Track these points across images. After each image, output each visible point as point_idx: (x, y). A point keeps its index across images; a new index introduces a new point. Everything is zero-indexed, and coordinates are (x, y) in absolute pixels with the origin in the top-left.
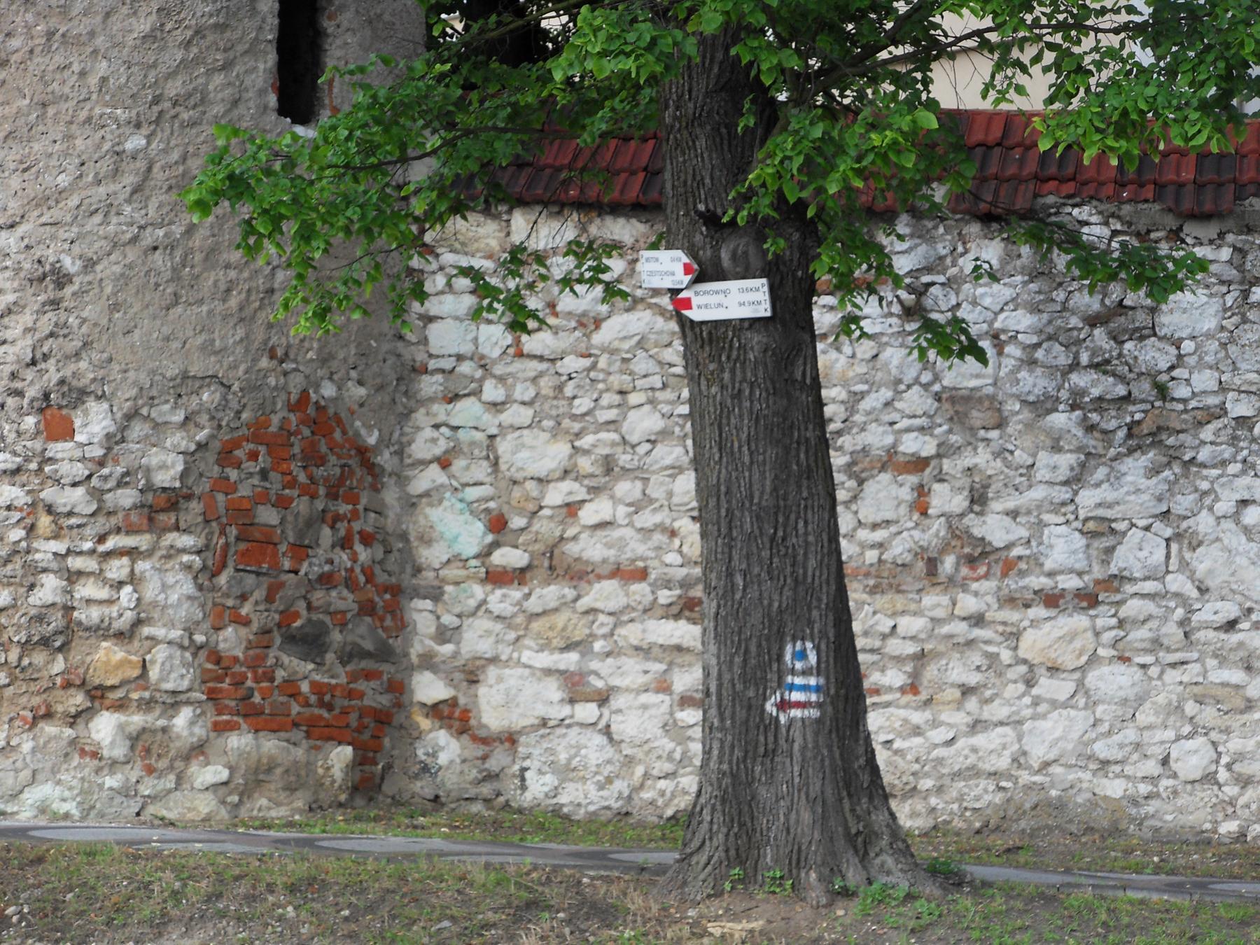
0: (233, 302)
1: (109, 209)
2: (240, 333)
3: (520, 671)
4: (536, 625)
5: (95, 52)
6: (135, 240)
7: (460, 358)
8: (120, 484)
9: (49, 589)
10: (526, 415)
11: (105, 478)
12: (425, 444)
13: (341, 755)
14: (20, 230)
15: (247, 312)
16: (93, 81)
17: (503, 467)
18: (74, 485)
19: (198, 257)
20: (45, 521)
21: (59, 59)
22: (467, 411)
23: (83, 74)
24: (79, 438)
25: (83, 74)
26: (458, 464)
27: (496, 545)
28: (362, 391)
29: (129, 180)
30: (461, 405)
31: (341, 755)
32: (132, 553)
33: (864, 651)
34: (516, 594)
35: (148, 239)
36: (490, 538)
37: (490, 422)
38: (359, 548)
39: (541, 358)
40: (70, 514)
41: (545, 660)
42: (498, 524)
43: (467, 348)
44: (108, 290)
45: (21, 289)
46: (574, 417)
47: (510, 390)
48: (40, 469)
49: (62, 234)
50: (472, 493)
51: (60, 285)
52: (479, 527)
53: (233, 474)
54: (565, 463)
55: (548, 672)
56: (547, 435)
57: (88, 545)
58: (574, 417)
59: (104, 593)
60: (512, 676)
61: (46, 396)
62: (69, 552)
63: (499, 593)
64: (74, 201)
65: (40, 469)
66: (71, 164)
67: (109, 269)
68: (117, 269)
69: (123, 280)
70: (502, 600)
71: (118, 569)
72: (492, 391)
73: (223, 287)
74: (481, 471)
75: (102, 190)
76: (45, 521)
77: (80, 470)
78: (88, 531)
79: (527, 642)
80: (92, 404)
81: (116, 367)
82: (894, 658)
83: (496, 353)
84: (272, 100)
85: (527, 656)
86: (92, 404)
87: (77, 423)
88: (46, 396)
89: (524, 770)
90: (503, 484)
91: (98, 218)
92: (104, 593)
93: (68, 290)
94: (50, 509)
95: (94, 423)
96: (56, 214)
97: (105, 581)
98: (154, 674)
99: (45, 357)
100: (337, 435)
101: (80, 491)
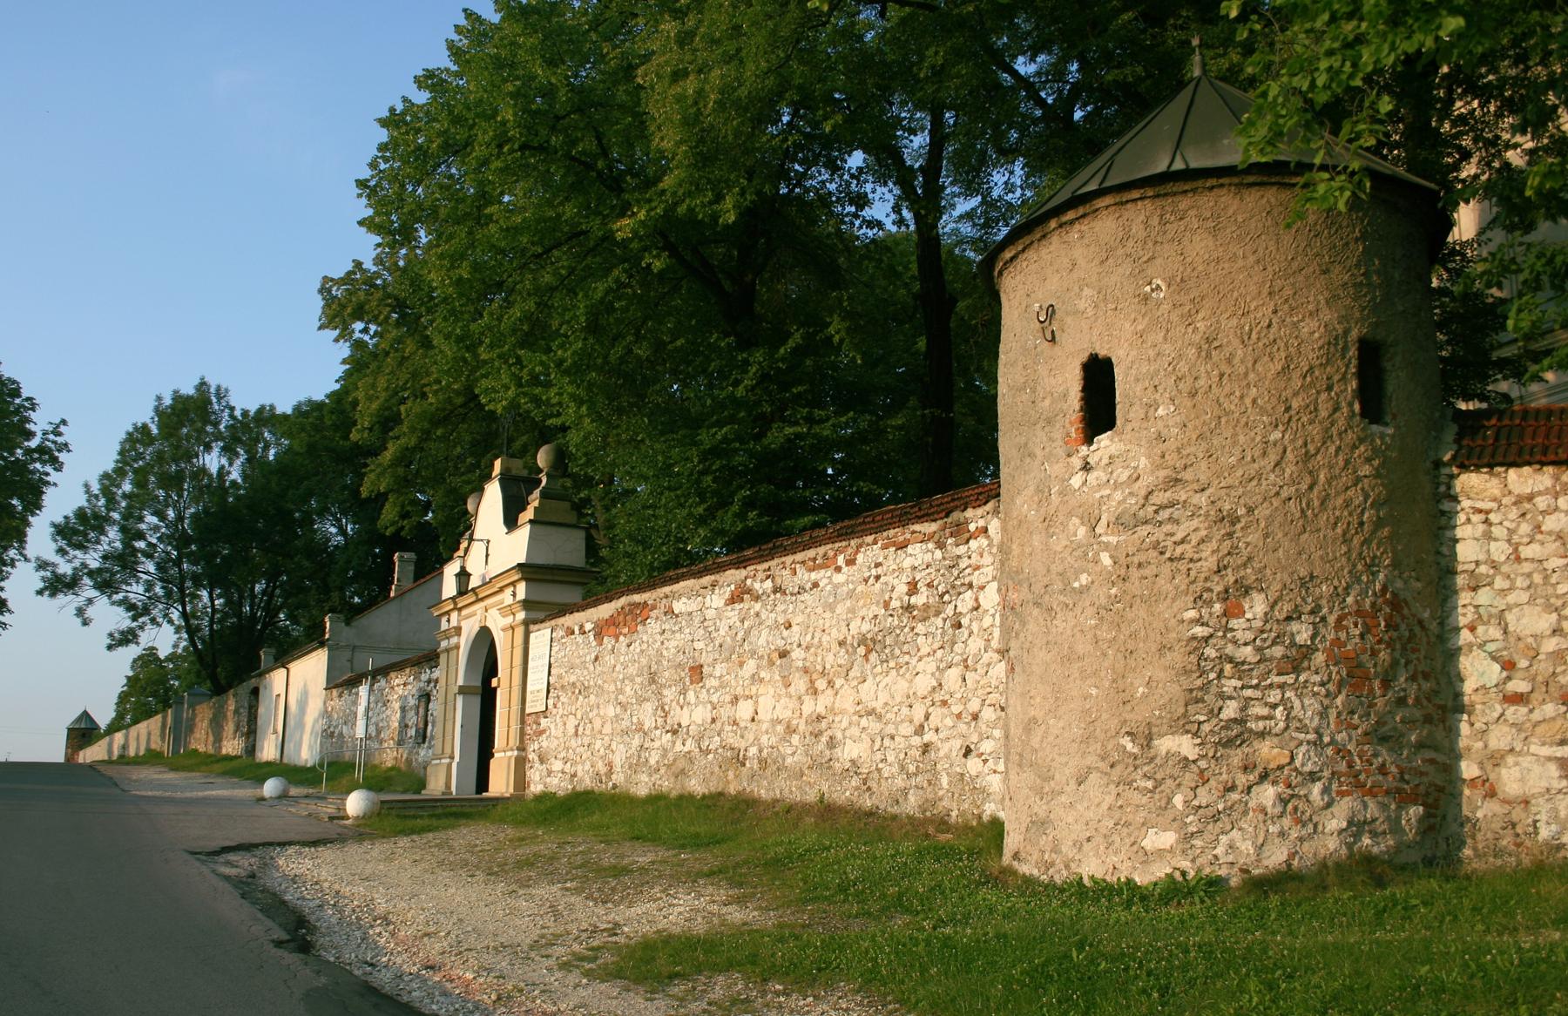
0: (1339, 530)
1: (1259, 476)
2: (1344, 549)
3: (1529, 758)
4: (1539, 730)
5: (1248, 385)
6: (1277, 494)
7: (1477, 563)
8: (1274, 643)
9: (1230, 710)
10: (1524, 597)
11: (1264, 640)
12: (1464, 617)
13: (1415, 811)
14: (1207, 492)
15: (1348, 536)
16: (1248, 401)
17: (1511, 628)
18: (1246, 644)
19: (1316, 503)
20: (1228, 667)
21: (1227, 389)
22: (1484, 597)
23: (1242, 397)
24: (1249, 615)
25: (1242, 397)
26: (1480, 629)
27: (1509, 678)
28: (1419, 585)
29: (1273, 457)
30: (1481, 591)
31: (1415, 811)
32: (1282, 686)
33: (127, 737)
34: (1524, 710)
35: (1285, 494)
36: (1505, 674)
37: (1501, 604)
38: (1421, 681)
39: (1533, 560)
40: (1243, 663)
41: (1546, 751)
42: (1509, 666)
43: (1482, 557)
44: (1262, 525)
45: (1210, 527)
46: (1558, 597)
47: (1513, 581)
48: (1224, 636)
49: (1233, 493)
50: (1491, 647)
51: (1233, 524)
52: (1497, 667)
53: (1343, 636)
54: (1554, 626)
55: (1549, 759)
56: (1539, 609)
57: (1255, 682)
58: (1558, 597)
59: (1265, 711)
60: (1526, 761)
61: (1226, 591)
62: (1242, 688)
63: (1513, 708)
64: (1239, 473)
65: (1224, 636)
66: (1237, 452)
67: (1262, 512)
68: (1268, 512)
69: (1270, 520)
70: (1516, 713)
71: (1274, 696)
72: (1499, 583)
73: (1332, 520)
74: (1494, 632)
75: (1256, 466)
76: (1228, 667)
77: (1249, 636)
78: (1255, 673)
79: (1533, 739)
80: (1255, 594)
81: (1268, 571)
82: (177, 741)
83: (1503, 558)
84: (975, 517)
85: (1533, 749)
86: (1255, 594)
87: (1247, 607)
88: (1226, 591)
89: (1536, 822)
90: (1512, 640)
91: (1254, 483)
92: (1265, 711)
93: (1238, 526)
94: (1231, 660)
95: (1257, 606)
96: (1229, 481)
97: (1266, 704)
98: (1298, 763)
99: (1225, 567)
100: (1406, 611)
101: (1249, 648)
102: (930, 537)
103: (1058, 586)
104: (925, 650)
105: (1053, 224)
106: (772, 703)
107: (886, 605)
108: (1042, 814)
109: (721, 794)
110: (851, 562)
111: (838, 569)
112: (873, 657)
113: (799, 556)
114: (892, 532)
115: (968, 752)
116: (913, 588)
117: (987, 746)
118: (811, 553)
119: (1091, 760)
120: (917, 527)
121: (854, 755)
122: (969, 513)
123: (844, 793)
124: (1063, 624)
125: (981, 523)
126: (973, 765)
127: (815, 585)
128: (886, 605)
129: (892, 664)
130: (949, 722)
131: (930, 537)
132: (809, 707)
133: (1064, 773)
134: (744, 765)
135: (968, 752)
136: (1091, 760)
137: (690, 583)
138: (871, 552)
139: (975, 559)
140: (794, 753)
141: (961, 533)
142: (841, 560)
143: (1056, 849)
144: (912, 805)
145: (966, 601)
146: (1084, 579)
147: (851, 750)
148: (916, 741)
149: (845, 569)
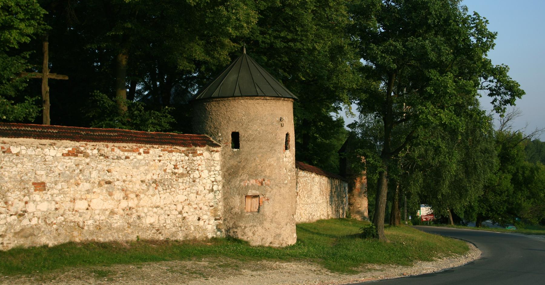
102: (183, 152)
103: (282, 182)
104: (182, 187)
105: (283, 99)
106: (100, 202)
107: (165, 170)
108: (279, 233)
109: (71, 243)
110: (147, 152)
111: (140, 154)
112: (160, 188)
113: (117, 144)
114: (166, 146)
115: (199, 219)
116: (175, 167)
117: (205, 217)
118: (124, 144)
119: (288, 220)
120: (178, 147)
121: (152, 221)
122: (198, 148)
123: (148, 235)
124: (283, 191)
125: (201, 152)
126: (201, 223)
127: (127, 158)
128: (165, 170)
129: (168, 191)
130: (192, 210)
131: (183, 152)
132: (124, 204)
133: (283, 224)
134: (83, 228)
135: (199, 219)
136: (288, 220)
137: (32, 140)
138: (156, 151)
139: (199, 162)
140: (118, 222)
141: (194, 153)
142: (141, 150)
143: (283, 240)
144: (180, 237)
145: (196, 174)
146: (286, 182)
147: (148, 221)
148: (180, 216)
149: (143, 154)
